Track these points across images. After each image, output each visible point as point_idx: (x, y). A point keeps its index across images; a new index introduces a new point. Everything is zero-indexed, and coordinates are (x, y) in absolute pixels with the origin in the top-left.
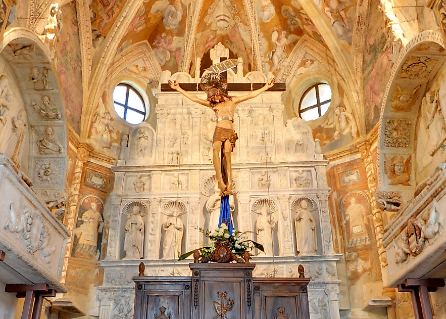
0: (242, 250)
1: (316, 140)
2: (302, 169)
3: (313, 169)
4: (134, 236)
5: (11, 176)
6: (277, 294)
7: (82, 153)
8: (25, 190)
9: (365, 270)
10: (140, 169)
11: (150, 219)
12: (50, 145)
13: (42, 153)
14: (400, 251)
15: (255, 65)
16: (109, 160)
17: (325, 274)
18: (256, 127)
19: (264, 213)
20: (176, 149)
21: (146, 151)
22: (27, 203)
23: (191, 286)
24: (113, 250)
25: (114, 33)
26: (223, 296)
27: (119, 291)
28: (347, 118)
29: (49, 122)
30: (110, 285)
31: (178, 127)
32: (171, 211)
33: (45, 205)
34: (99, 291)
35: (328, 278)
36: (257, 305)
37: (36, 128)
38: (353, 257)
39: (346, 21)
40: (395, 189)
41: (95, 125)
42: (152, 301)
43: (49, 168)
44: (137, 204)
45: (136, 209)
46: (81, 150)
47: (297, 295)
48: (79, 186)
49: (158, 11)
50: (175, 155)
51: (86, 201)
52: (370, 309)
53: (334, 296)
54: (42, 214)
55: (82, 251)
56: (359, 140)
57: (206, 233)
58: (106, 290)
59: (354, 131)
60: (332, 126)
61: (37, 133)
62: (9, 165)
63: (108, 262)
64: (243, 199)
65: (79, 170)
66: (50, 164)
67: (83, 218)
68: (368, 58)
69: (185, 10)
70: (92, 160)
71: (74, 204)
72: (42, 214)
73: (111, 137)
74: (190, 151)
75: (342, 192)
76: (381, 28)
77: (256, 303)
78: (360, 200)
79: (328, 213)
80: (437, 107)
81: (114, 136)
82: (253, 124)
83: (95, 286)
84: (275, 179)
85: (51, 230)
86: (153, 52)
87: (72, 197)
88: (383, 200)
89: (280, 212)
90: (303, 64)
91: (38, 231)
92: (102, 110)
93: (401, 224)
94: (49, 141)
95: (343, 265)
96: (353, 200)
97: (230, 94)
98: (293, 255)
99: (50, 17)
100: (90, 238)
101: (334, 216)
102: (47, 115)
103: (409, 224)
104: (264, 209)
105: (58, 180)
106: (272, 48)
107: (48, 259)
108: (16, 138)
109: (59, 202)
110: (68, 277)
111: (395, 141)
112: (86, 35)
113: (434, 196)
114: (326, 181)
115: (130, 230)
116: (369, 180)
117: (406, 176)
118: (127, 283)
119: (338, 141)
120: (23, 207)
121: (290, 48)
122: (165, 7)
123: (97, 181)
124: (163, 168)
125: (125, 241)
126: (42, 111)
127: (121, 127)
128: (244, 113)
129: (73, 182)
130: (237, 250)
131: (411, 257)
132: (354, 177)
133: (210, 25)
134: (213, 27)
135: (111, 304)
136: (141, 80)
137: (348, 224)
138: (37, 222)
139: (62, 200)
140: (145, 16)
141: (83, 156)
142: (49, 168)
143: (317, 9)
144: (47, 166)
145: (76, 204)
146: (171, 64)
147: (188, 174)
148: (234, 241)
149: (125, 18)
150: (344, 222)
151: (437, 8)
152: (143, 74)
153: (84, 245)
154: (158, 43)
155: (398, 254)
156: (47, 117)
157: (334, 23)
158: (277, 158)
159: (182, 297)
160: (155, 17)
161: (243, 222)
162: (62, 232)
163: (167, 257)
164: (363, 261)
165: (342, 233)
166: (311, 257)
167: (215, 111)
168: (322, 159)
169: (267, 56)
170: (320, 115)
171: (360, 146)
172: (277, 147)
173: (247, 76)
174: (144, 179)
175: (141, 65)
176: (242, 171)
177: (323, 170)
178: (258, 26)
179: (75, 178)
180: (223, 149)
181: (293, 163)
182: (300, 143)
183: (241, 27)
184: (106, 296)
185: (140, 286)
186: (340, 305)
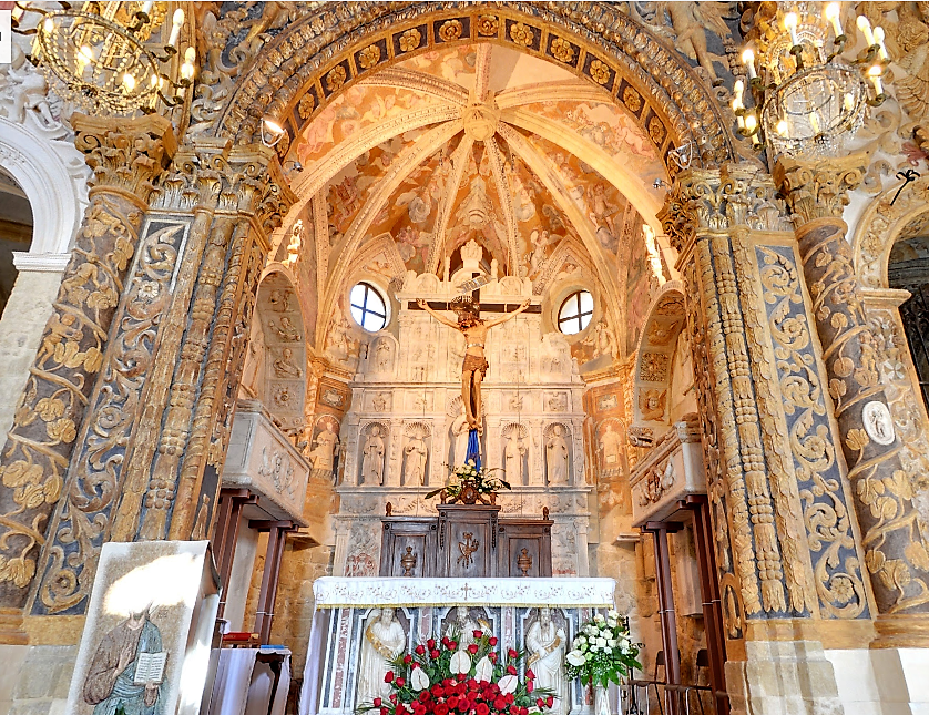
0: (489, 489)
3: (568, 391)
4: (373, 460)
7: (317, 368)
9: (616, 504)
10: (381, 386)
11: (391, 442)
12: (288, 368)
15: (511, 268)
16: (346, 375)
17: (575, 505)
19: (515, 438)
20: (419, 364)
21: (388, 365)
22: (276, 444)
23: (436, 526)
24: (350, 475)
26: (469, 537)
28: (608, 336)
31: (423, 337)
35: (579, 511)
36: (501, 545)
39: (612, 228)
40: (647, 425)
41: (331, 334)
44: (376, 424)
45: (375, 430)
46: (316, 363)
50: (420, 370)
52: (618, 544)
53: (583, 529)
57: (451, 468)
58: (344, 519)
59: (615, 351)
60: (592, 344)
63: (345, 488)
64: (492, 422)
65: (314, 387)
68: (633, 273)
69: (435, 205)
70: (327, 375)
73: (348, 348)
74: (435, 366)
75: (598, 418)
78: (616, 428)
81: (352, 346)
84: (528, 400)
86: (396, 245)
89: (531, 438)
90: (565, 268)
92: (338, 318)
93: (645, 469)
95: (594, 497)
96: (609, 428)
97: (483, 315)
99: (294, 236)
100: (326, 462)
102: (285, 337)
104: (514, 434)
106: (530, 250)
112: (323, 232)
113: (670, 451)
119: (597, 360)
120: (274, 449)
121: (550, 248)
123: (333, 398)
124: (405, 386)
127: (360, 335)
130: (484, 489)
132: (611, 402)
133: (462, 220)
134: (465, 223)
136: (383, 279)
137: (602, 453)
143: (581, 214)
146: (416, 261)
148: (481, 480)
149: (367, 214)
152: (384, 272)
158: (531, 378)
159: (428, 537)
160: (400, 209)
161: (492, 459)
165: (595, 463)
166: (562, 488)
167: (466, 335)
168: (578, 380)
170: (581, 329)
172: (531, 365)
174: (384, 396)
175: (382, 261)
177: (579, 393)
178: (516, 226)
180: (472, 379)
181: (547, 384)
183: (497, 225)
185: (386, 526)
186: (589, 539)
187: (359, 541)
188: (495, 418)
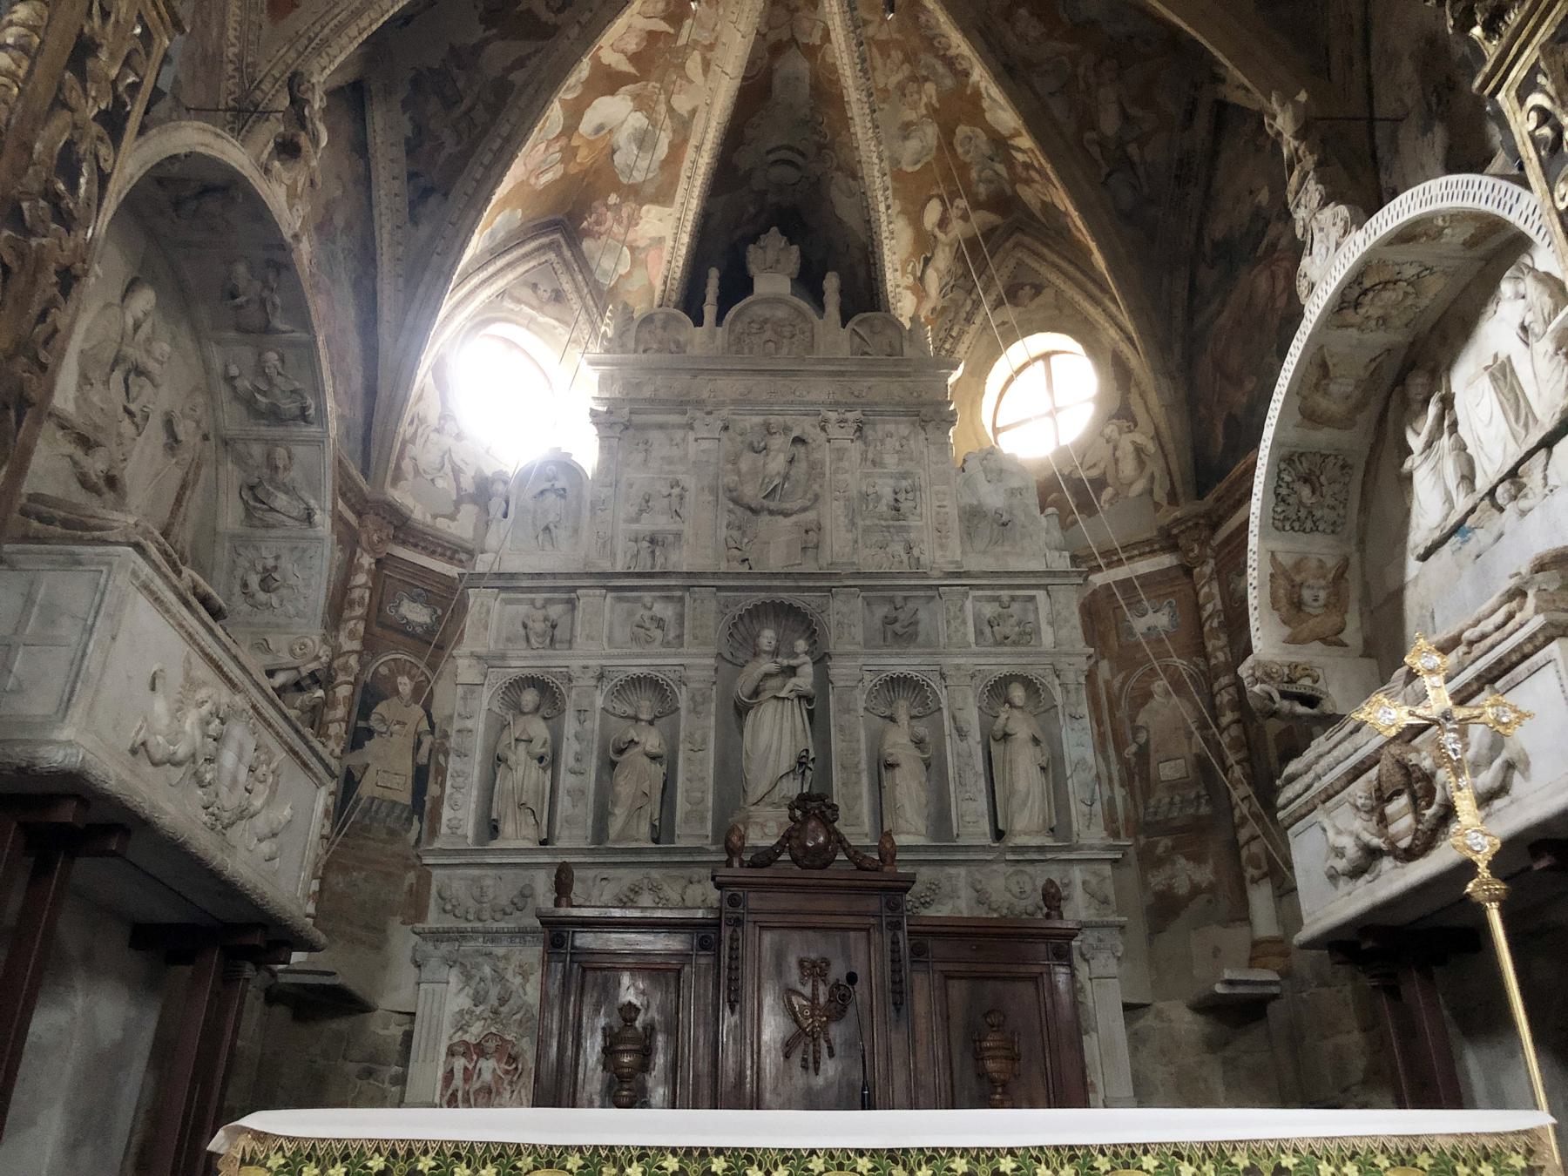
1: (1050, 510)
5: (158, 584)
8: (202, 631)
12: (281, 501)
14: (1347, 842)
22: (203, 671)
25: (481, 170)
29: (277, 432)
30: (449, 922)
32: (631, 704)
36: (921, 1003)
37: (240, 447)
38: (1160, 850)
42: (595, 984)
48: (361, 627)
49: (600, 128)
50: (646, 544)
51: (384, 671)
54: (254, 707)
58: (438, 936)
61: (240, 461)
62: (152, 550)
63: (443, 852)
66: (277, 558)
67: (374, 722)
72: (254, 707)
76: (1251, 192)
77: (916, 994)
79: (1086, 721)
80: (1441, 418)
82: (869, 463)
83: (403, 923)
85: (281, 755)
88: (1266, 687)
91: (240, 759)
94: (277, 488)
103: (1386, 761)
105: (301, 607)
108: (178, 474)
109: (305, 672)
111: (1303, 513)
114: (1080, 630)
116: (1206, 628)
117: (1335, 619)
118: (498, 916)
120: (191, 683)
122: (622, 117)
125: (496, 790)
129: (346, 614)
131: (1387, 863)
135: (453, 979)
138: (237, 731)
139: (313, 666)
140: (563, 142)
141: (375, 538)
142: (276, 568)
145: (352, 679)
147: (681, 599)
150: (1133, 748)
151: (1513, 93)
154: (598, 223)
155: (1339, 852)
156: (274, 416)
157: (1109, 175)
160: (590, 143)
163: (618, 839)
164: (1191, 865)
166: (1041, 849)
169: (910, 268)
171: (1182, 532)
173: (850, 325)
176: (837, 593)
179: (352, 604)
187: (478, 1000)
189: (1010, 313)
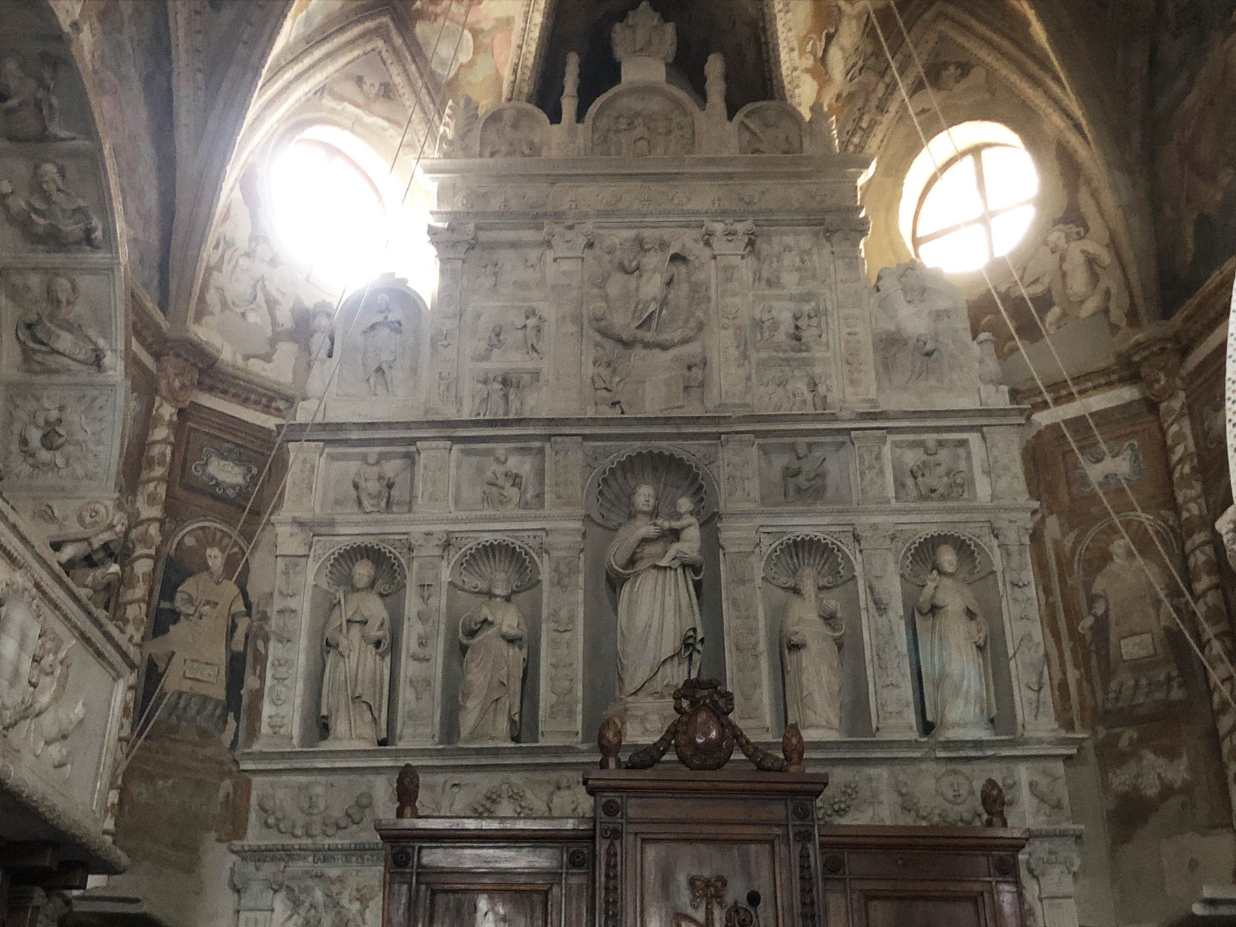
1: (983, 336)
2: (935, 436)
3: (973, 438)
6: (910, 886)
12: (65, 341)
13: (38, 368)
18: (774, 292)
27: (305, 859)
29: (59, 259)
30: (272, 839)
33: (47, 553)
34: (235, 858)
38: (1124, 743)
42: (447, 909)
43: (60, 421)
46: (171, 364)
47: (982, 894)
48: (162, 490)
50: (497, 386)
51: (190, 541)
54: (37, 586)
55: (174, 717)
56: (1140, 337)
58: (259, 855)
63: (264, 756)
71: (146, 551)
79: (1032, 591)
82: (763, 283)
83: (219, 840)
87: (141, 529)
91: (22, 646)
98: (914, 735)
101: (1051, 600)
107: (56, 752)
110: (126, 808)
114: (1022, 477)
115: (343, 643)
116: (1177, 475)
126: (34, 217)
128: (731, 244)
129: (145, 475)
139: (107, 536)
141: (177, 384)
142: (60, 421)
144: (55, 414)
145: (152, 552)
147: (541, 451)
150: (1088, 621)
153: (180, 694)
156: (54, 240)
162: (109, 650)
166: (978, 744)
169: (809, 48)
173: (739, 116)
179: (151, 463)
182: (929, 347)
184: (261, 875)
188: (744, 523)
189: (932, 98)
